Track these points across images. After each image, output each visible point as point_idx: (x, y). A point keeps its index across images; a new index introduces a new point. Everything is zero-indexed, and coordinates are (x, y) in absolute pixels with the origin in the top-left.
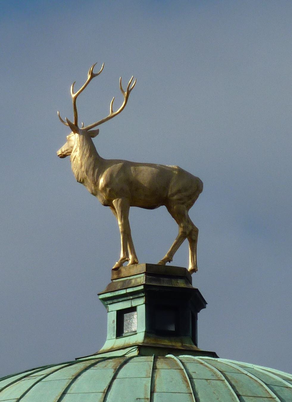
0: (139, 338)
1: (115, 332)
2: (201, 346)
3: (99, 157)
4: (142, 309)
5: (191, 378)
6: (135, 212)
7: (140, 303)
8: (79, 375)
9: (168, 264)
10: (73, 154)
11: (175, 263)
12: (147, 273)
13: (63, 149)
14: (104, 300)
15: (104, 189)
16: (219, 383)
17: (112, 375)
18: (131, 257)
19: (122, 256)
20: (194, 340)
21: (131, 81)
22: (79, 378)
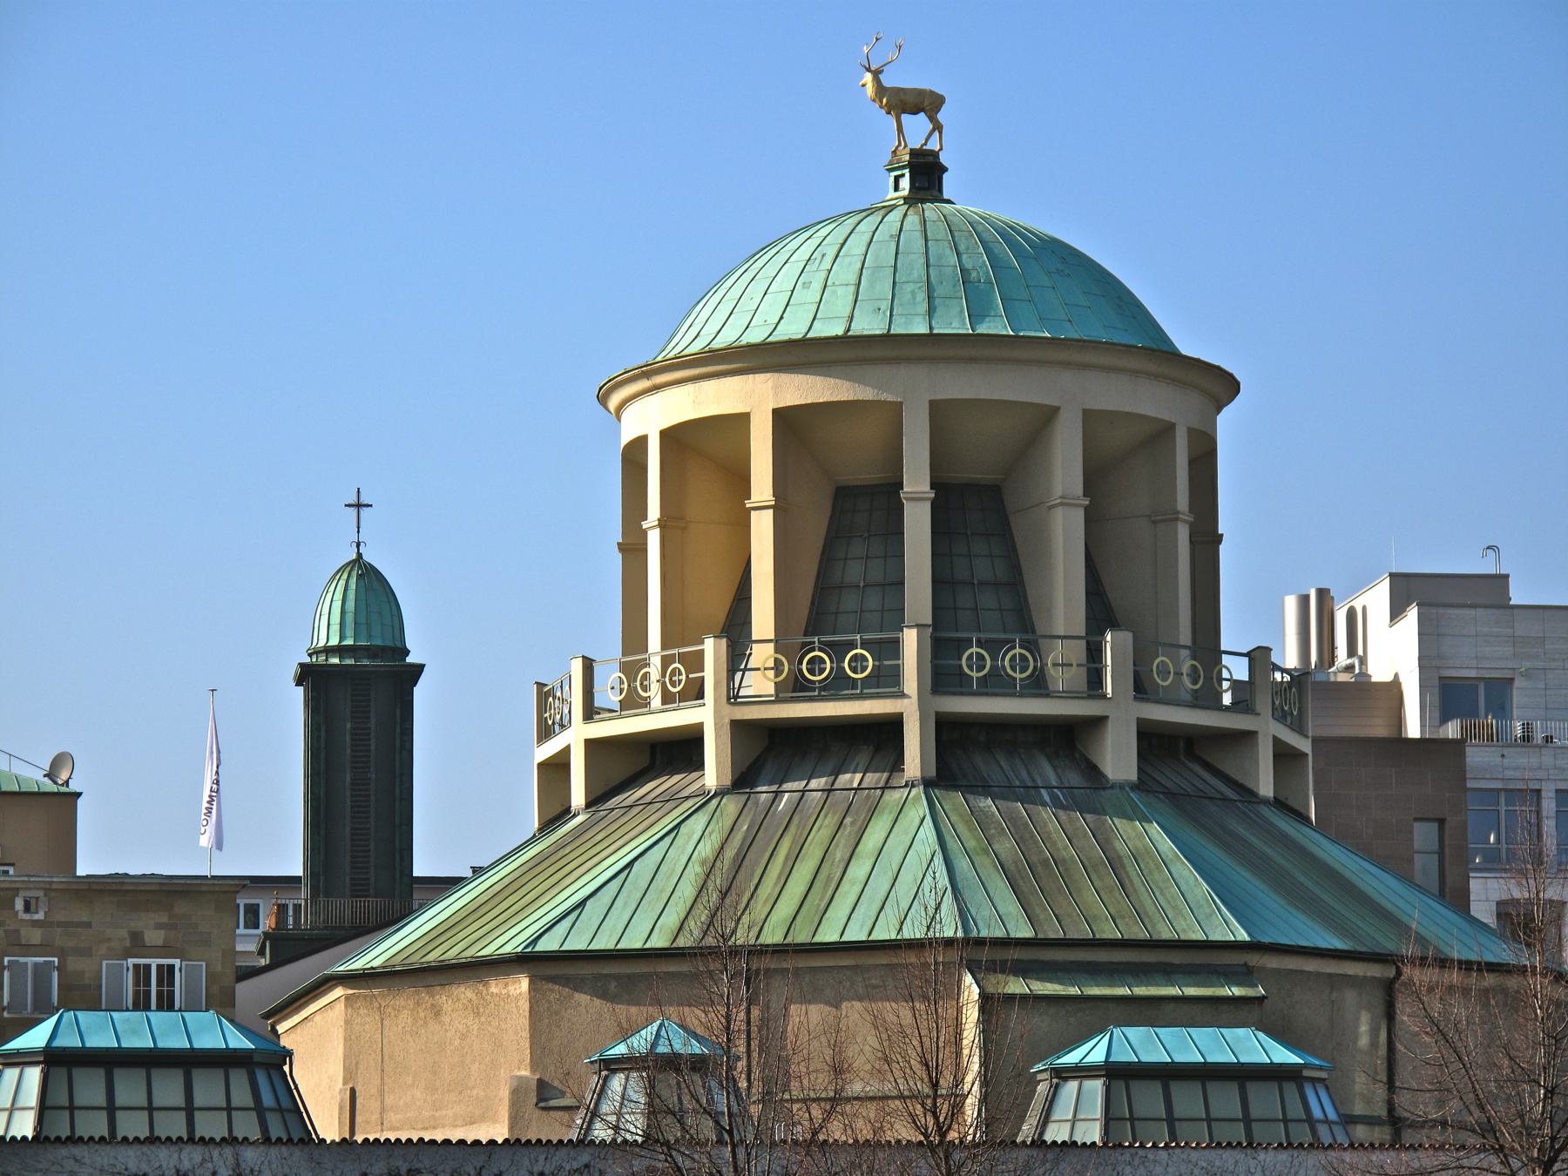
0: (906, 193)
1: (242, 1039)
2: (946, 196)
4: (907, 175)
5: (925, 221)
6: (905, 118)
7: (906, 171)
9: (924, 147)
10: (867, 86)
11: (929, 147)
12: (910, 154)
14: (887, 170)
15: (886, 105)
16: (941, 223)
17: (880, 220)
18: (903, 143)
20: (940, 190)
22: (862, 223)
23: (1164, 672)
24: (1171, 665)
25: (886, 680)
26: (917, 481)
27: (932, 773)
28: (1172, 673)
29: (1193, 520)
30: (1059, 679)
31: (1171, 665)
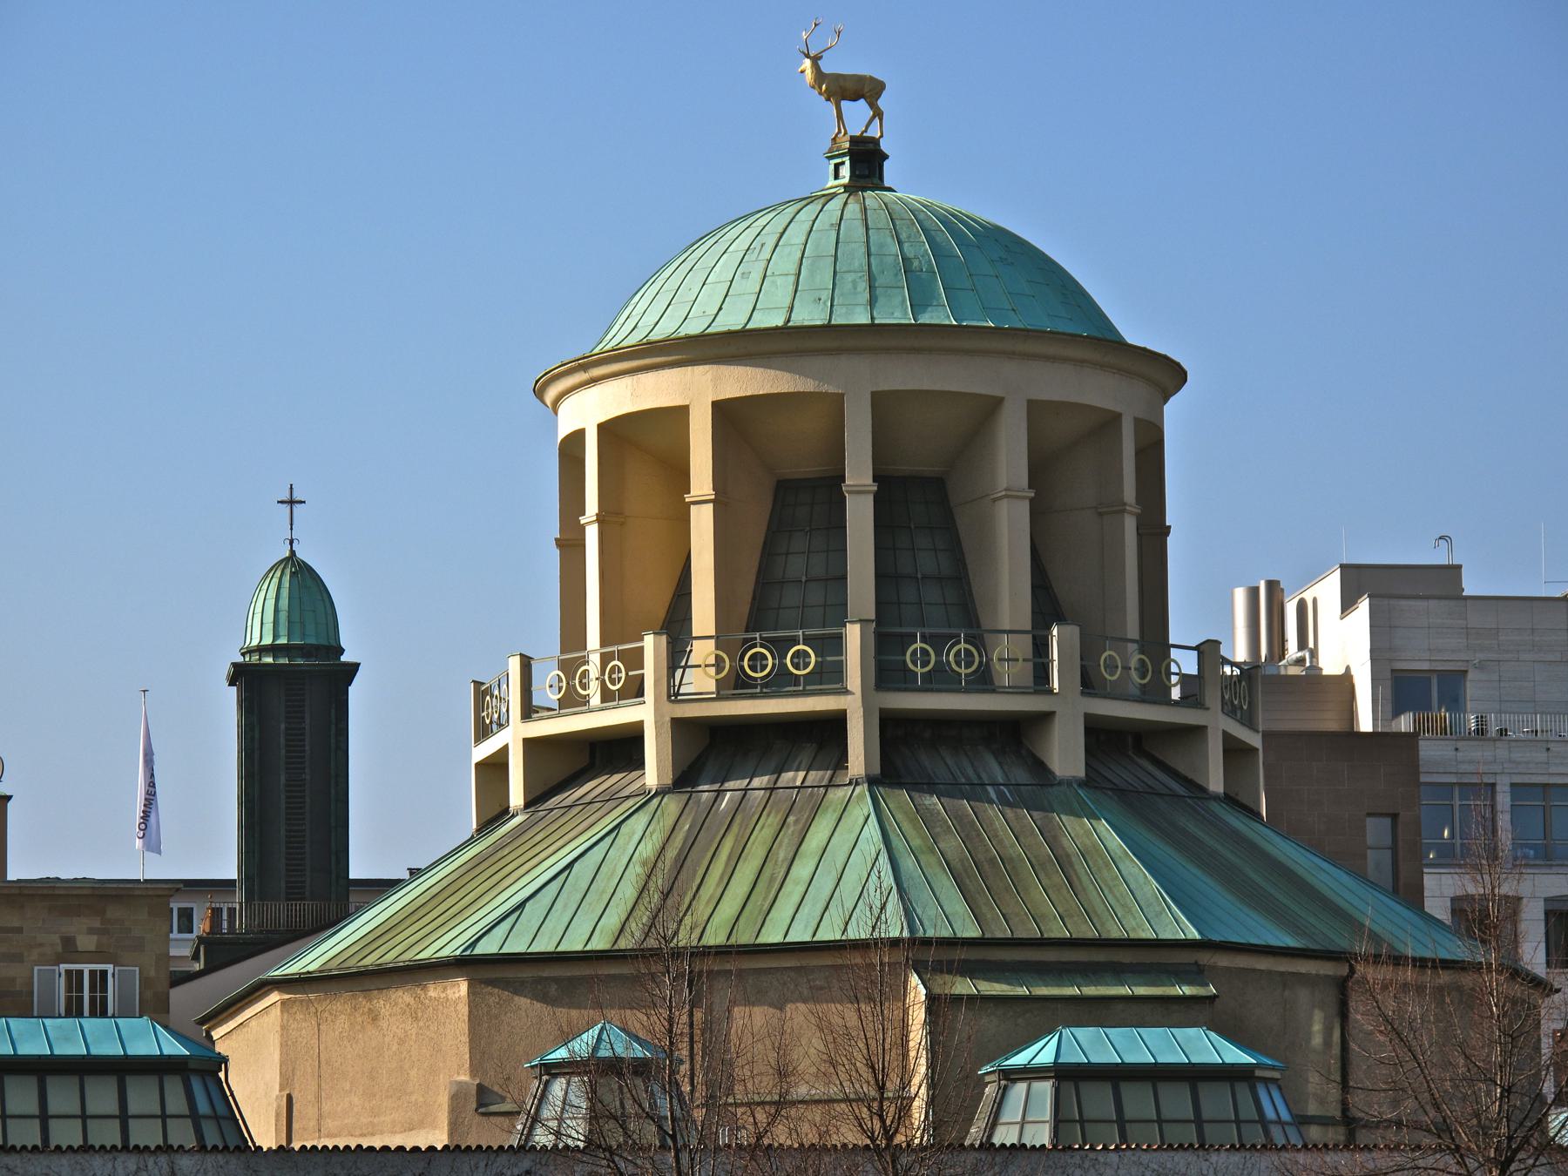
0: (846, 180)
2: (887, 184)
3: (822, 72)
5: (865, 209)
6: (845, 104)
7: (847, 159)
8: (801, 209)
9: (865, 135)
10: (806, 72)
12: (850, 142)
13: (802, 68)
15: (825, 91)
16: (882, 211)
17: (820, 208)
18: (843, 131)
19: (837, 131)
20: (881, 178)
21: (840, 26)
23: (1111, 667)
24: (1117, 658)
25: (829, 676)
26: (859, 474)
27: (877, 770)
28: (1120, 668)
29: (1140, 511)
30: (1005, 674)
31: (1117, 658)
